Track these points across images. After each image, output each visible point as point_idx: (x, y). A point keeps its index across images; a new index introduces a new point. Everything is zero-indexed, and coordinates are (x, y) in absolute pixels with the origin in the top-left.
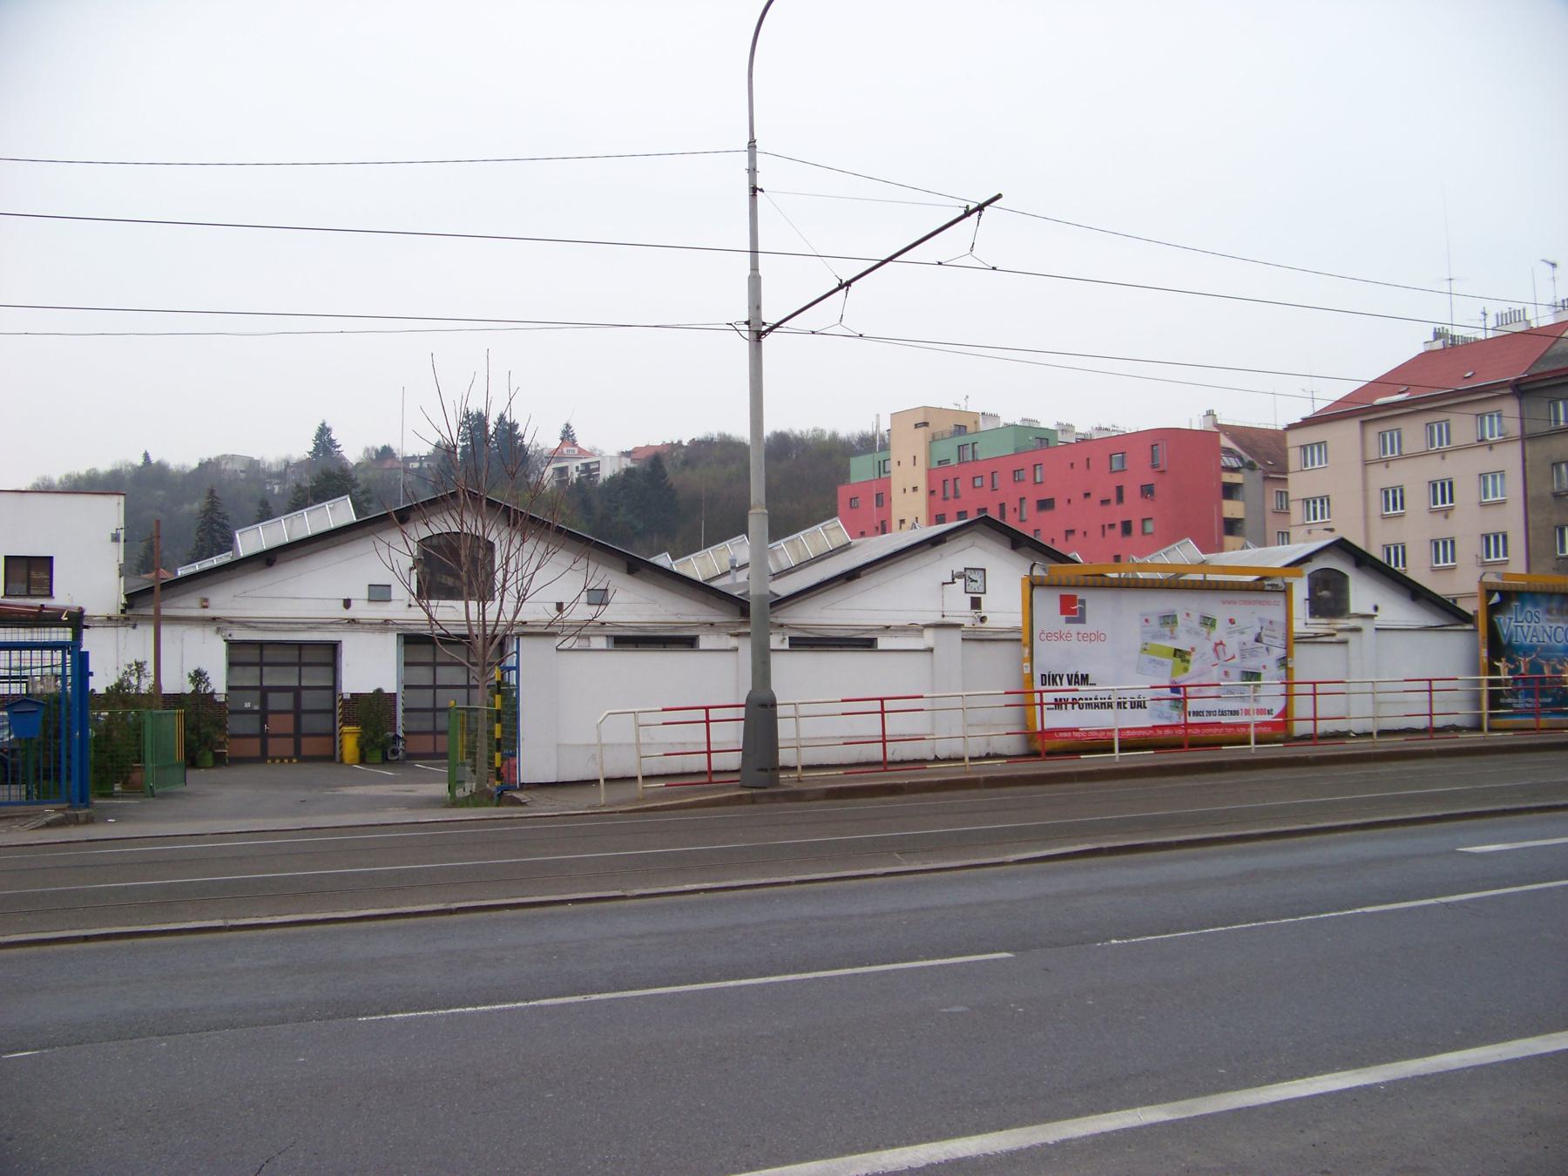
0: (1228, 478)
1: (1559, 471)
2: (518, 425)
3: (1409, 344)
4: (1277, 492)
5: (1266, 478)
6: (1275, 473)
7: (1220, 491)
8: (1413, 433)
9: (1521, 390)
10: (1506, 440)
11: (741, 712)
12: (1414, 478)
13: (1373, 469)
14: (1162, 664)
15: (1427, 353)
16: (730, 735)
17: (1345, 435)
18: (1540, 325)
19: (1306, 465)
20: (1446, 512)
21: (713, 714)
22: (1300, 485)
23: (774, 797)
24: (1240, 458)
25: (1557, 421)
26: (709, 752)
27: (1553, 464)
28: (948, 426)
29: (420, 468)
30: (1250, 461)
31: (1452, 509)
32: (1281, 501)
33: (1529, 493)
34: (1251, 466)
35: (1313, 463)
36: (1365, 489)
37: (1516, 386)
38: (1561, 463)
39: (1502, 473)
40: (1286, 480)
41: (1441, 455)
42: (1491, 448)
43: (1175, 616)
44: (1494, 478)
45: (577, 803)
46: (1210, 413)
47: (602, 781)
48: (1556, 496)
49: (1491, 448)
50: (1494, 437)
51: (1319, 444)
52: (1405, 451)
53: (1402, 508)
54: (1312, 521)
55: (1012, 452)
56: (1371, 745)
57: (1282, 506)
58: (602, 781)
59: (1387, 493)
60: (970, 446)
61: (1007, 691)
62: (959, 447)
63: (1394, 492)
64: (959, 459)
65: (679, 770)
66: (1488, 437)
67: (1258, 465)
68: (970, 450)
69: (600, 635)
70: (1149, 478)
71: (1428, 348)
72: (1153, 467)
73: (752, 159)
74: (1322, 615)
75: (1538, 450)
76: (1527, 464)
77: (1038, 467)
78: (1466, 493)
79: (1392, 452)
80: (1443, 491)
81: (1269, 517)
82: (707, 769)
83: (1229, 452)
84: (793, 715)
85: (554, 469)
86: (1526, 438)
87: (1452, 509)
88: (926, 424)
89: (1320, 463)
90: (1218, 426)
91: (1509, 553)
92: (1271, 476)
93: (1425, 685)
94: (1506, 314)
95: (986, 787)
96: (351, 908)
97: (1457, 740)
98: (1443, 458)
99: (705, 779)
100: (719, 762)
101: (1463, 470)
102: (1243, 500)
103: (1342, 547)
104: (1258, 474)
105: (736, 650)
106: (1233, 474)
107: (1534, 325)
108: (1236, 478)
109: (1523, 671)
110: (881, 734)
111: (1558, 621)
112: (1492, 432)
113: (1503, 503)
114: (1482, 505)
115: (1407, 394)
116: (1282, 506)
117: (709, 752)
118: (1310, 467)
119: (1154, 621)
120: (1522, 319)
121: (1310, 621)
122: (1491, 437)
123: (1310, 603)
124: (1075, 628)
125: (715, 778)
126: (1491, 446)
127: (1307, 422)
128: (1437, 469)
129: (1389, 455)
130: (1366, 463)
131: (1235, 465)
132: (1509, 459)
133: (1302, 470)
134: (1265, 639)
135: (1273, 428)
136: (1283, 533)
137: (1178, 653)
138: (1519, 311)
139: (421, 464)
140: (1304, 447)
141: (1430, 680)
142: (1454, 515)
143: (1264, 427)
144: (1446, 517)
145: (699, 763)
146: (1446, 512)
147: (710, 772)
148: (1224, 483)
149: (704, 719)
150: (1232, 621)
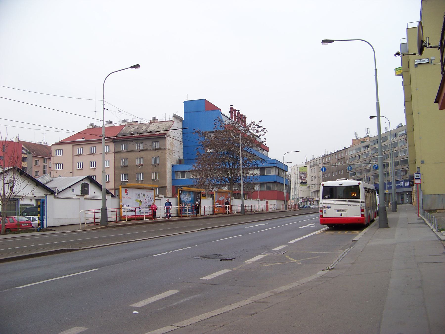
0: (23, 155)
1: (122, 161)
3: (83, 126)
4: (36, 160)
5: (33, 156)
6: (36, 155)
8: (86, 149)
10: (110, 153)
11: (100, 211)
12: (86, 160)
13: (75, 157)
14: (138, 203)
15: (88, 129)
16: (99, 215)
17: (68, 148)
19: (56, 155)
20: (94, 169)
22: (55, 159)
23: (107, 227)
24: (26, 150)
25: (122, 149)
26: (94, 219)
27: (121, 159)
30: (29, 152)
31: (96, 168)
32: (36, 163)
34: (29, 153)
35: (58, 155)
36: (73, 162)
37: (114, 140)
38: (123, 159)
39: (109, 161)
40: (51, 159)
41: (93, 155)
43: (140, 194)
44: (106, 161)
45: (75, 228)
48: (122, 167)
51: (61, 150)
53: (82, 167)
54: (57, 169)
57: (36, 164)
59: (78, 163)
63: (80, 163)
65: (71, 224)
67: (31, 153)
69: (110, 195)
71: (88, 128)
73: (104, 102)
75: (118, 156)
79: (80, 153)
80: (94, 164)
81: (33, 167)
83: (24, 149)
86: (115, 152)
87: (96, 168)
90: (19, 141)
92: (35, 156)
95: (135, 225)
96: (113, 242)
100: (97, 220)
104: (31, 155)
105: (80, 199)
108: (26, 156)
109: (5, 210)
111: (188, 196)
113: (109, 168)
115: (85, 139)
116: (36, 164)
117: (94, 219)
118: (57, 155)
119: (137, 195)
124: (127, 196)
127: (57, 144)
128: (93, 158)
129: (79, 154)
130: (73, 156)
131: (25, 152)
132: (111, 157)
133: (55, 156)
134: (151, 199)
135: (33, 143)
136: (36, 171)
137: (140, 201)
140: (56, 150)
142: (96, 170)
143: (31, 142)
144: (94, 170)
145: (93, 221)
146: (94, 169)
147: (95, 223)
149: (94, 212)
150: (147, 195)
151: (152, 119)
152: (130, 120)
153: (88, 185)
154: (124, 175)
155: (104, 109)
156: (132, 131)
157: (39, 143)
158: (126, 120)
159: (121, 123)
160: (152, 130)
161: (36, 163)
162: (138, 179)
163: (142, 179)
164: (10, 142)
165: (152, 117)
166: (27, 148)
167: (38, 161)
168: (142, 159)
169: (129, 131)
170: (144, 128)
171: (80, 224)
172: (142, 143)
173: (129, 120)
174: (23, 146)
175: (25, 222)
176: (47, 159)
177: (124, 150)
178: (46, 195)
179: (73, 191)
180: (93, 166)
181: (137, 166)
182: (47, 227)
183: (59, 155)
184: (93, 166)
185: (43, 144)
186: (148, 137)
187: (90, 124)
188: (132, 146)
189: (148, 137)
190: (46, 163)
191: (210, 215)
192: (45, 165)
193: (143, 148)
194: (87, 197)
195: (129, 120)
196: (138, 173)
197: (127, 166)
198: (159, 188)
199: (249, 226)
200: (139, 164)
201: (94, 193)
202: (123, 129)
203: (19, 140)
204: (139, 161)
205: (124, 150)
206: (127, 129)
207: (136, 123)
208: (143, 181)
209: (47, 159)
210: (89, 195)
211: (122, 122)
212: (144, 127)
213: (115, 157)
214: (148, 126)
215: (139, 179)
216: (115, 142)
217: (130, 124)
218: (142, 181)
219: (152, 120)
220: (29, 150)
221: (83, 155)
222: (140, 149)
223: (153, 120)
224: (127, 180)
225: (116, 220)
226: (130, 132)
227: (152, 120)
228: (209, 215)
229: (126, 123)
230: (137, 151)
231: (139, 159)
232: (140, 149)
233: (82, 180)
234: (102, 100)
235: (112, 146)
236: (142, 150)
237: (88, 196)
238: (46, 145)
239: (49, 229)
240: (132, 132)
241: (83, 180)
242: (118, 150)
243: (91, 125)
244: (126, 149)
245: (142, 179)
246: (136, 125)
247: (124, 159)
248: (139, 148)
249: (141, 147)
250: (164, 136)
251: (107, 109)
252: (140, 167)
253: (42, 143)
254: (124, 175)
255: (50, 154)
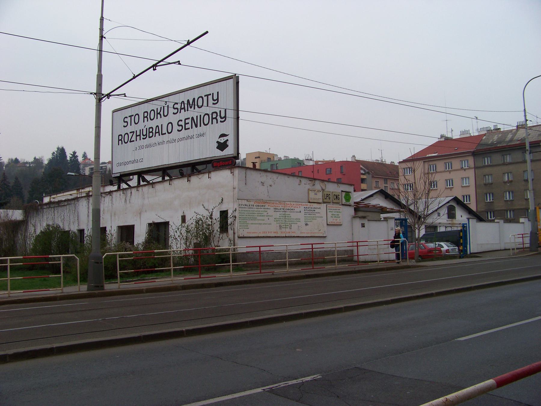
0: (363, 177)
2: (76, 152)
5: (373, 177)
6: (375, 175)
7: (360, 181)
8: (440, 165)
9: (475, 154)
10: (470, 168)
11: (529, 235)
15: (439, 141)
17: (419, 166)
18: (474, 135)
21: (524, 236)
28: (265, 158)
29: (30, 166)
32: (377, 184)
33: (477, 184)
34: (368, 173)
35: (407, 173)
38: (486, 175)
39: (468, 178)
42: (465, 170)
44: (466, 179)
46: (354, 156)
47: (515, 249)
48: (485, 185)
49: (465, 170)
50: (466, 167)
52: (438, 170)
55: (291, 167)
56: (7, 295)
58: (515, 249)
60: (275, 165)
61: (385, 240)
62: (271, 165)
64: (271, 169)
66: (464, 167)
67: (370, 173)
68: (275, 166)
70: (340, 176)
71: (439, 140)
72: (341, 173)
74: (450, 218)
76: (476, 175)
77: (300, 172)
78: (457, 183)
82: (357, 260)
83: (361, 169)
84: (335, 247)
85: (89, 168)
86: (475, 168)
88: (259, 157)
89: (409, 173)
91: (471, 201)
92: (375, 176)
93: (521, 236)
94: (463, 131)
97: (324, 269)
98: (450, 173)
99: (522, 250)
101: (456, 176)
102: (366, 184)
103: (456, 199)
104: (371, 176)
105: (499, 222)
106: (364, 176)
107: (472, 135)
108: (364, 177)
110: (522, 241)
112: (465, 166)
113: (469, 186)
114: (462, 187)
115: (437, 154)
117: (523, 244)
120: (468, 133)
121: (448, 220)
122: (465, 167)
123: (448, 215)
125: (525, 249)
126: (465, 170)
127: (405, 161)
128: (447, 176)
129: (432, 171)
131: (364, 173)
132: (471, 174)
135: (371, 161)
138: (467, 131)
139: (30, 165)
140: (404, 169)
141: (522, 234)
142: (453, 190)
143: (368, 161)
144: (451, 190)
145: (521, 246)
147: (523, 248)
148: (361, 178)
151: (519, 125)
152: (491, 128)
153: (455, 207)
154: (488, 194)
155: (527, 120)
156: (494, 141)
157: (377, 162)
158: (486, 128)
159: (479, 131)
160: (521, 138)
161: (377, 184)
162: (506, 198)
163: (511, 199)
164: (347, 162)
165: (519, 122)
166: (365, 168)
167: (378, 182)
168: (511, 174)
169: (491, 140)
170: (510, 136)
171: (511, 249)
172: (509, 154)
173: (489, 127)
174: (361, 166)
175: (435, 249)
176: (388, 180)
177: (486, 164)
178: (468, 219)
179: (439, 215)
180: (450, 186)
181: (505, 183)
182: (471, 253)
183: (408, 174)
184: (450, 186)
185: (382, 163)
186: (518, 146)
187: (441, 136)
188: (497, 158)
189: (518, 146)
190: (387, 184)
191: (380, 261)
192: (385, 186)
193: (511, 161)
194: (454, 221)
195: (490, 127)
196: (506, 192)
197: (492, 184)
198: (513, 211)
199: (376, 288)
200: (507, 180)
201: (461, 216)
202: (483, 138)
203: (356, 159)
204: (507, 176)
205: (486, 164)
206: (487, 138)
207: (499, 131)
208: (513, 200)
209: (388, 180)
210: (456, 219)
211: (480, 131)
212: (510, 135)
213: (476, 173)
214: (515, 134)
215: (508, 199)
216: (475, 155)
217: (491, 132)
218: (511, 200)
219: (524, 124)
220: (368, 170)
221: (436, 172)
222: (508, 162)
223: (521, 125)
224: (493, 200)
225: (357, 260)
226: (492, 141)
227: (524, 124)
228: (376, 261)
229: (486, 132)
230: (504, 164)
231: (506, 174)
232: (507, 161)
233: (448, 202)
234: (523, 110)
235: (471, 160)
236: (510, 164)
237: (455, 220)
238: (384, 163)
239: (474, 255)
240: (495, 142)
241: (450, 202)
242: (480, 164)
243: (442, 136)
244: (489, 163)
245: (511, 199)
246: (499, 133)
247: (487, 175)
248: (506, 160)
249: (508, 159)
250: (538, 145)
251: (531, 121)
252: (508, 184)
253: (380, 161)
254: (488, 194)
255: (390, 173)
